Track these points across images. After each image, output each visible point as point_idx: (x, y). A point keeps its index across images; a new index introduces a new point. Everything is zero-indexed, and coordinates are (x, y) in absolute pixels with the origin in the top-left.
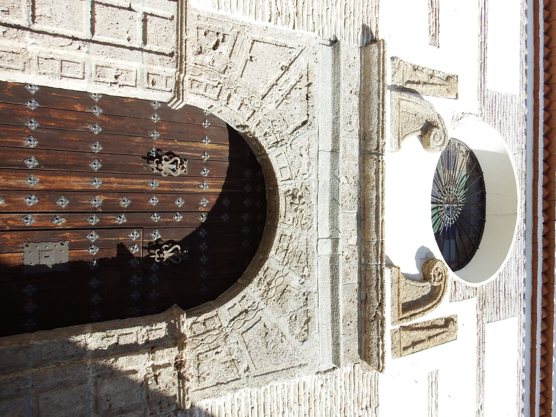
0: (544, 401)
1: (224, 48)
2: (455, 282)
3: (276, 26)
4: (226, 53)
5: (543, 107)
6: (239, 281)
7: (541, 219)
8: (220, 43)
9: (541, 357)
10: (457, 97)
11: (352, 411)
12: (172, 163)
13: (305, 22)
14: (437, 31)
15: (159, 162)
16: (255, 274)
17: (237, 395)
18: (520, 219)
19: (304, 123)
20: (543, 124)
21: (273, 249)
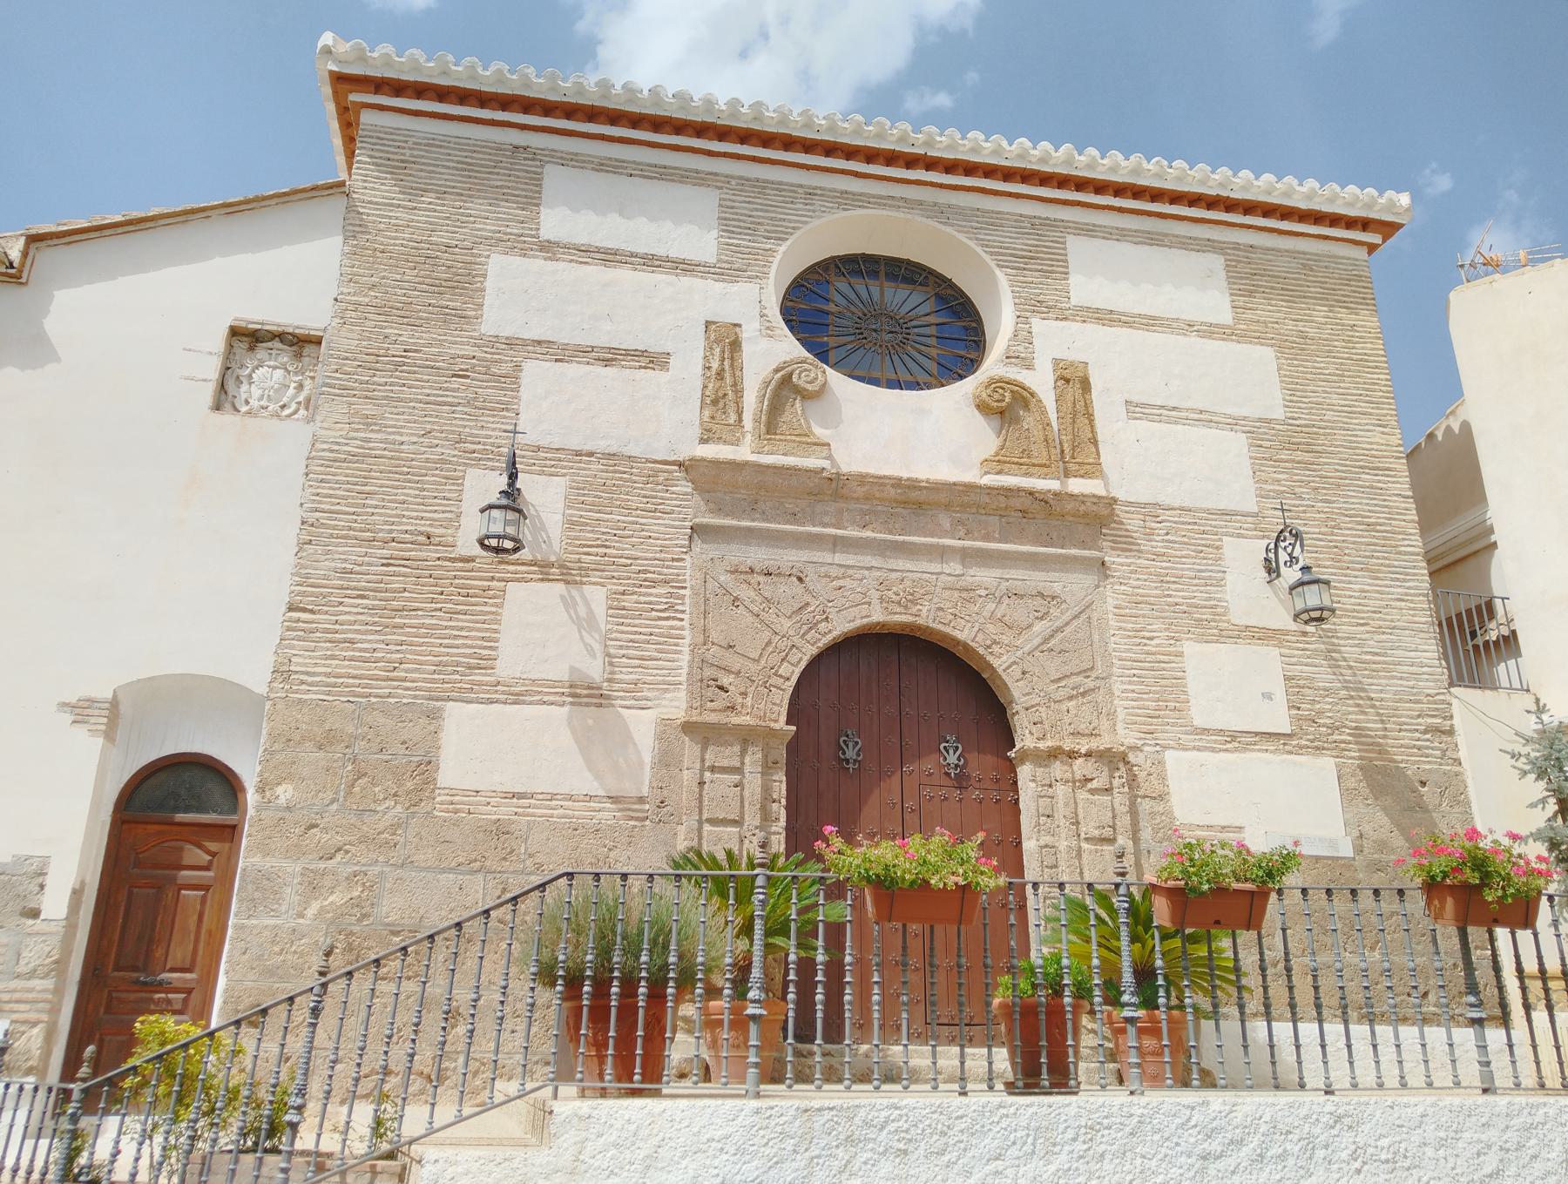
0: (901, 162)
1: (726, 680)
2: (1007, 357)
3: (688, 612)
4: (731, 678)
5: (716, 142)
6: (985, 676)
7: (1249, 220)
8: (719, 683)
9: (786, 150)
10: (708, 324)
11: (1159, 544)
12: (847, 746)
13: (676, 571)
14: (645, 354)
15: (847, 761)
16: (982, 657)
17: (1117, 693)
18: (890, 213)
19: (800, 579)
20: (570, 122)
21: (954, 634)
